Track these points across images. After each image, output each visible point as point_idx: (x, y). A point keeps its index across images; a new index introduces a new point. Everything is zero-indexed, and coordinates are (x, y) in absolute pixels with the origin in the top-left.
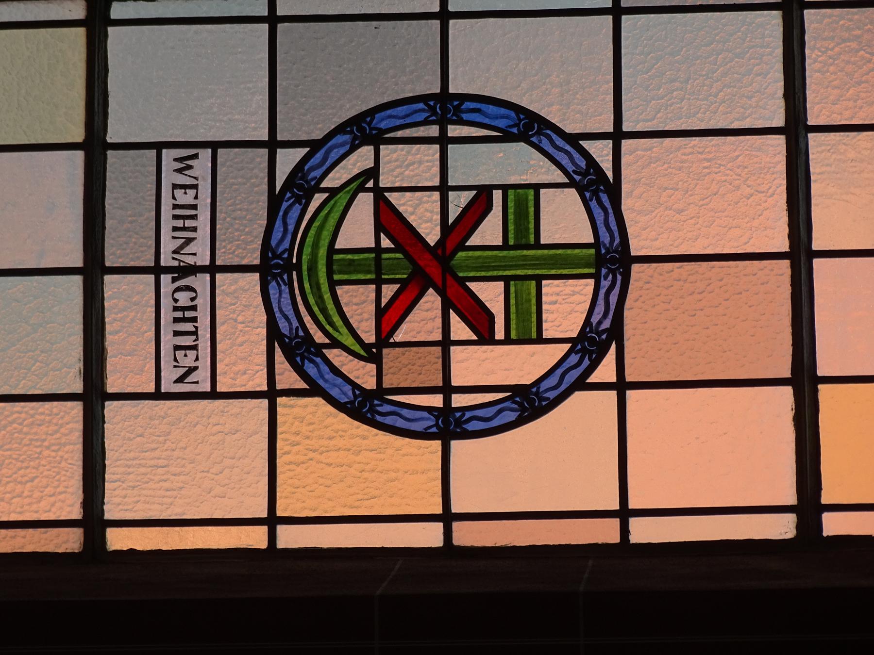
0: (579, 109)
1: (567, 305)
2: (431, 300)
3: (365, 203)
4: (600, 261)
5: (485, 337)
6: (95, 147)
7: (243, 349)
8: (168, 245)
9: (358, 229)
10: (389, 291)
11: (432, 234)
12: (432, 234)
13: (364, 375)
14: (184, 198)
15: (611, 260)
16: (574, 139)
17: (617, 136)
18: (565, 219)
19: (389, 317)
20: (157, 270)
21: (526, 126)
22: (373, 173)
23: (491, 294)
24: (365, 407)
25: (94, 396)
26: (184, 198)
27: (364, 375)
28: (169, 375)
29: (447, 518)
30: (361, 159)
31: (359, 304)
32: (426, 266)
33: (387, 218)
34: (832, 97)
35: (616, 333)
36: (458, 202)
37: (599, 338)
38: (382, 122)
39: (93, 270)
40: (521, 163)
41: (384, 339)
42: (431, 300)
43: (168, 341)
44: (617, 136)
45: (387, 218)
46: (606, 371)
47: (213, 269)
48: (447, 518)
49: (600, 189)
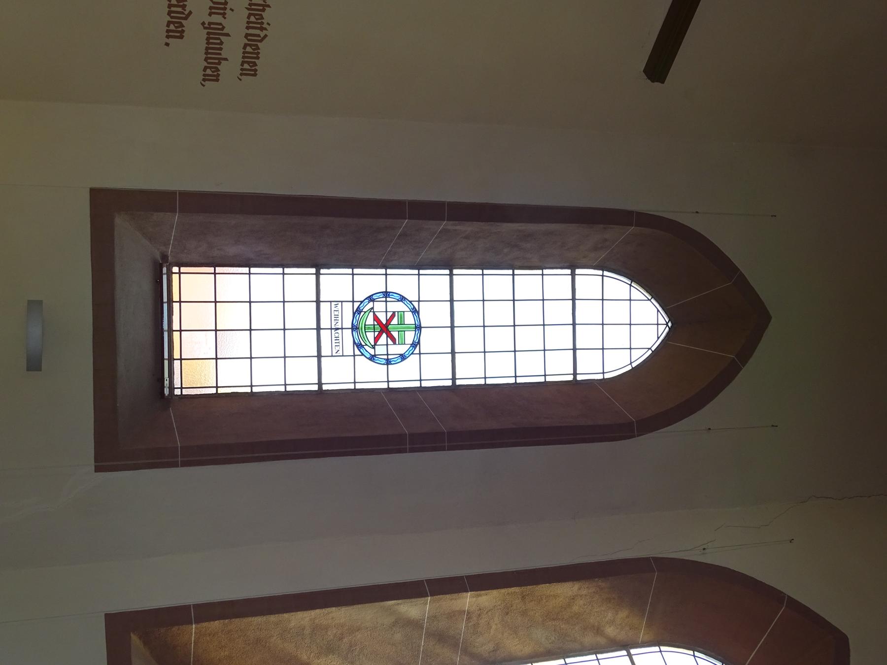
0: (412, 296)
1: (410, 337)
2: (384, 335)
3: (371, 314)
4: (416, 328)
5: (395, 343)
6: (318, 302)
7: (349, 348)
8: (333, 323)
9: (370, 321)
10: (376, 333)
11: (384, 322)
12: (384, 322)
13: (372, 352)
14: (336, 313)
15: (418, 328)
16: (411, 302)
17: (419, 301)
18: (409, 319)
19: (376, 339)
20: (331, 329)
21: (402, 299)
22: (373, 308)
23: (395, 334)
24: (372, 358)
25: (319, 356)
26: (336, 313)
27: (372, 352)
28: (334, 352)
29: (483, 275)
30: (371, 305)
31: (371, 336)
32: (384, 328)
33: (376, 318)
34: (582, 602)
35: (419, 343)
36: (389, 315)
37: (415, 344)
38: (374, 297)
39: (318, 329)
40: (399, 307)
41: (375, 344)
42: (384, 335)
43: (334, 344)
44: (419, 301)
45: (376, 318)
46: (417, 351)
47: (342, 329)
48: (483, 275)
49: (415, 312)
